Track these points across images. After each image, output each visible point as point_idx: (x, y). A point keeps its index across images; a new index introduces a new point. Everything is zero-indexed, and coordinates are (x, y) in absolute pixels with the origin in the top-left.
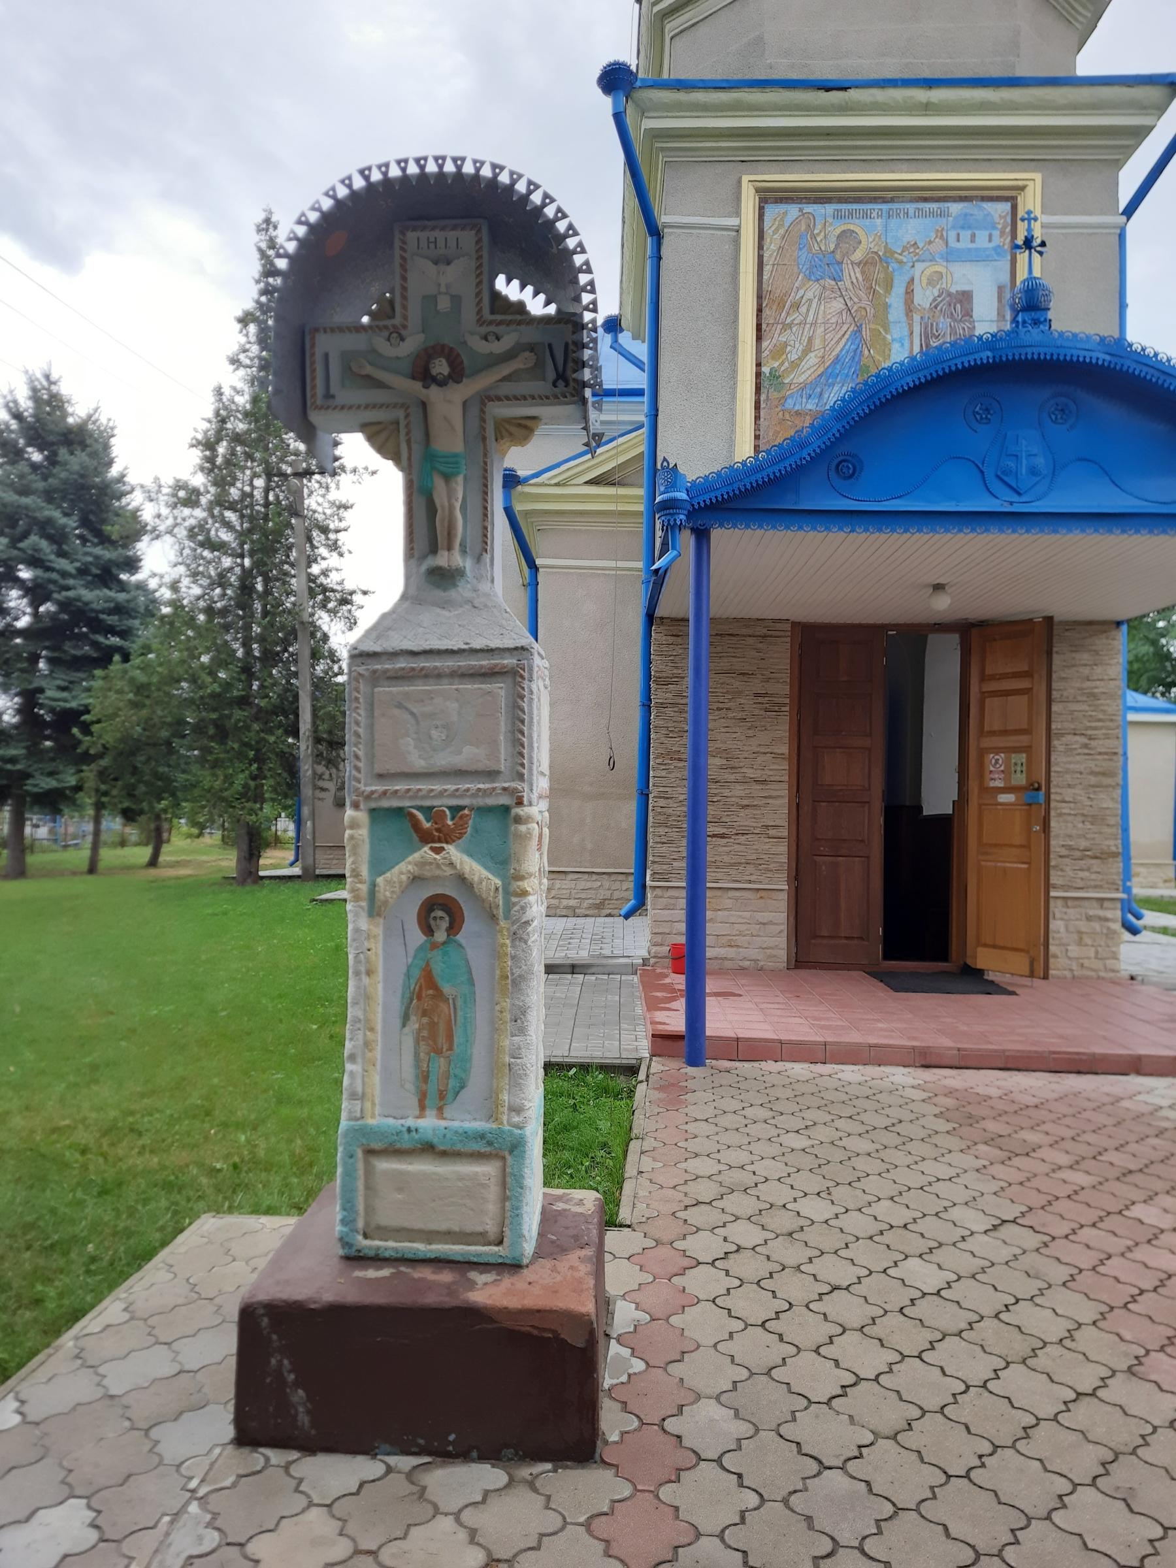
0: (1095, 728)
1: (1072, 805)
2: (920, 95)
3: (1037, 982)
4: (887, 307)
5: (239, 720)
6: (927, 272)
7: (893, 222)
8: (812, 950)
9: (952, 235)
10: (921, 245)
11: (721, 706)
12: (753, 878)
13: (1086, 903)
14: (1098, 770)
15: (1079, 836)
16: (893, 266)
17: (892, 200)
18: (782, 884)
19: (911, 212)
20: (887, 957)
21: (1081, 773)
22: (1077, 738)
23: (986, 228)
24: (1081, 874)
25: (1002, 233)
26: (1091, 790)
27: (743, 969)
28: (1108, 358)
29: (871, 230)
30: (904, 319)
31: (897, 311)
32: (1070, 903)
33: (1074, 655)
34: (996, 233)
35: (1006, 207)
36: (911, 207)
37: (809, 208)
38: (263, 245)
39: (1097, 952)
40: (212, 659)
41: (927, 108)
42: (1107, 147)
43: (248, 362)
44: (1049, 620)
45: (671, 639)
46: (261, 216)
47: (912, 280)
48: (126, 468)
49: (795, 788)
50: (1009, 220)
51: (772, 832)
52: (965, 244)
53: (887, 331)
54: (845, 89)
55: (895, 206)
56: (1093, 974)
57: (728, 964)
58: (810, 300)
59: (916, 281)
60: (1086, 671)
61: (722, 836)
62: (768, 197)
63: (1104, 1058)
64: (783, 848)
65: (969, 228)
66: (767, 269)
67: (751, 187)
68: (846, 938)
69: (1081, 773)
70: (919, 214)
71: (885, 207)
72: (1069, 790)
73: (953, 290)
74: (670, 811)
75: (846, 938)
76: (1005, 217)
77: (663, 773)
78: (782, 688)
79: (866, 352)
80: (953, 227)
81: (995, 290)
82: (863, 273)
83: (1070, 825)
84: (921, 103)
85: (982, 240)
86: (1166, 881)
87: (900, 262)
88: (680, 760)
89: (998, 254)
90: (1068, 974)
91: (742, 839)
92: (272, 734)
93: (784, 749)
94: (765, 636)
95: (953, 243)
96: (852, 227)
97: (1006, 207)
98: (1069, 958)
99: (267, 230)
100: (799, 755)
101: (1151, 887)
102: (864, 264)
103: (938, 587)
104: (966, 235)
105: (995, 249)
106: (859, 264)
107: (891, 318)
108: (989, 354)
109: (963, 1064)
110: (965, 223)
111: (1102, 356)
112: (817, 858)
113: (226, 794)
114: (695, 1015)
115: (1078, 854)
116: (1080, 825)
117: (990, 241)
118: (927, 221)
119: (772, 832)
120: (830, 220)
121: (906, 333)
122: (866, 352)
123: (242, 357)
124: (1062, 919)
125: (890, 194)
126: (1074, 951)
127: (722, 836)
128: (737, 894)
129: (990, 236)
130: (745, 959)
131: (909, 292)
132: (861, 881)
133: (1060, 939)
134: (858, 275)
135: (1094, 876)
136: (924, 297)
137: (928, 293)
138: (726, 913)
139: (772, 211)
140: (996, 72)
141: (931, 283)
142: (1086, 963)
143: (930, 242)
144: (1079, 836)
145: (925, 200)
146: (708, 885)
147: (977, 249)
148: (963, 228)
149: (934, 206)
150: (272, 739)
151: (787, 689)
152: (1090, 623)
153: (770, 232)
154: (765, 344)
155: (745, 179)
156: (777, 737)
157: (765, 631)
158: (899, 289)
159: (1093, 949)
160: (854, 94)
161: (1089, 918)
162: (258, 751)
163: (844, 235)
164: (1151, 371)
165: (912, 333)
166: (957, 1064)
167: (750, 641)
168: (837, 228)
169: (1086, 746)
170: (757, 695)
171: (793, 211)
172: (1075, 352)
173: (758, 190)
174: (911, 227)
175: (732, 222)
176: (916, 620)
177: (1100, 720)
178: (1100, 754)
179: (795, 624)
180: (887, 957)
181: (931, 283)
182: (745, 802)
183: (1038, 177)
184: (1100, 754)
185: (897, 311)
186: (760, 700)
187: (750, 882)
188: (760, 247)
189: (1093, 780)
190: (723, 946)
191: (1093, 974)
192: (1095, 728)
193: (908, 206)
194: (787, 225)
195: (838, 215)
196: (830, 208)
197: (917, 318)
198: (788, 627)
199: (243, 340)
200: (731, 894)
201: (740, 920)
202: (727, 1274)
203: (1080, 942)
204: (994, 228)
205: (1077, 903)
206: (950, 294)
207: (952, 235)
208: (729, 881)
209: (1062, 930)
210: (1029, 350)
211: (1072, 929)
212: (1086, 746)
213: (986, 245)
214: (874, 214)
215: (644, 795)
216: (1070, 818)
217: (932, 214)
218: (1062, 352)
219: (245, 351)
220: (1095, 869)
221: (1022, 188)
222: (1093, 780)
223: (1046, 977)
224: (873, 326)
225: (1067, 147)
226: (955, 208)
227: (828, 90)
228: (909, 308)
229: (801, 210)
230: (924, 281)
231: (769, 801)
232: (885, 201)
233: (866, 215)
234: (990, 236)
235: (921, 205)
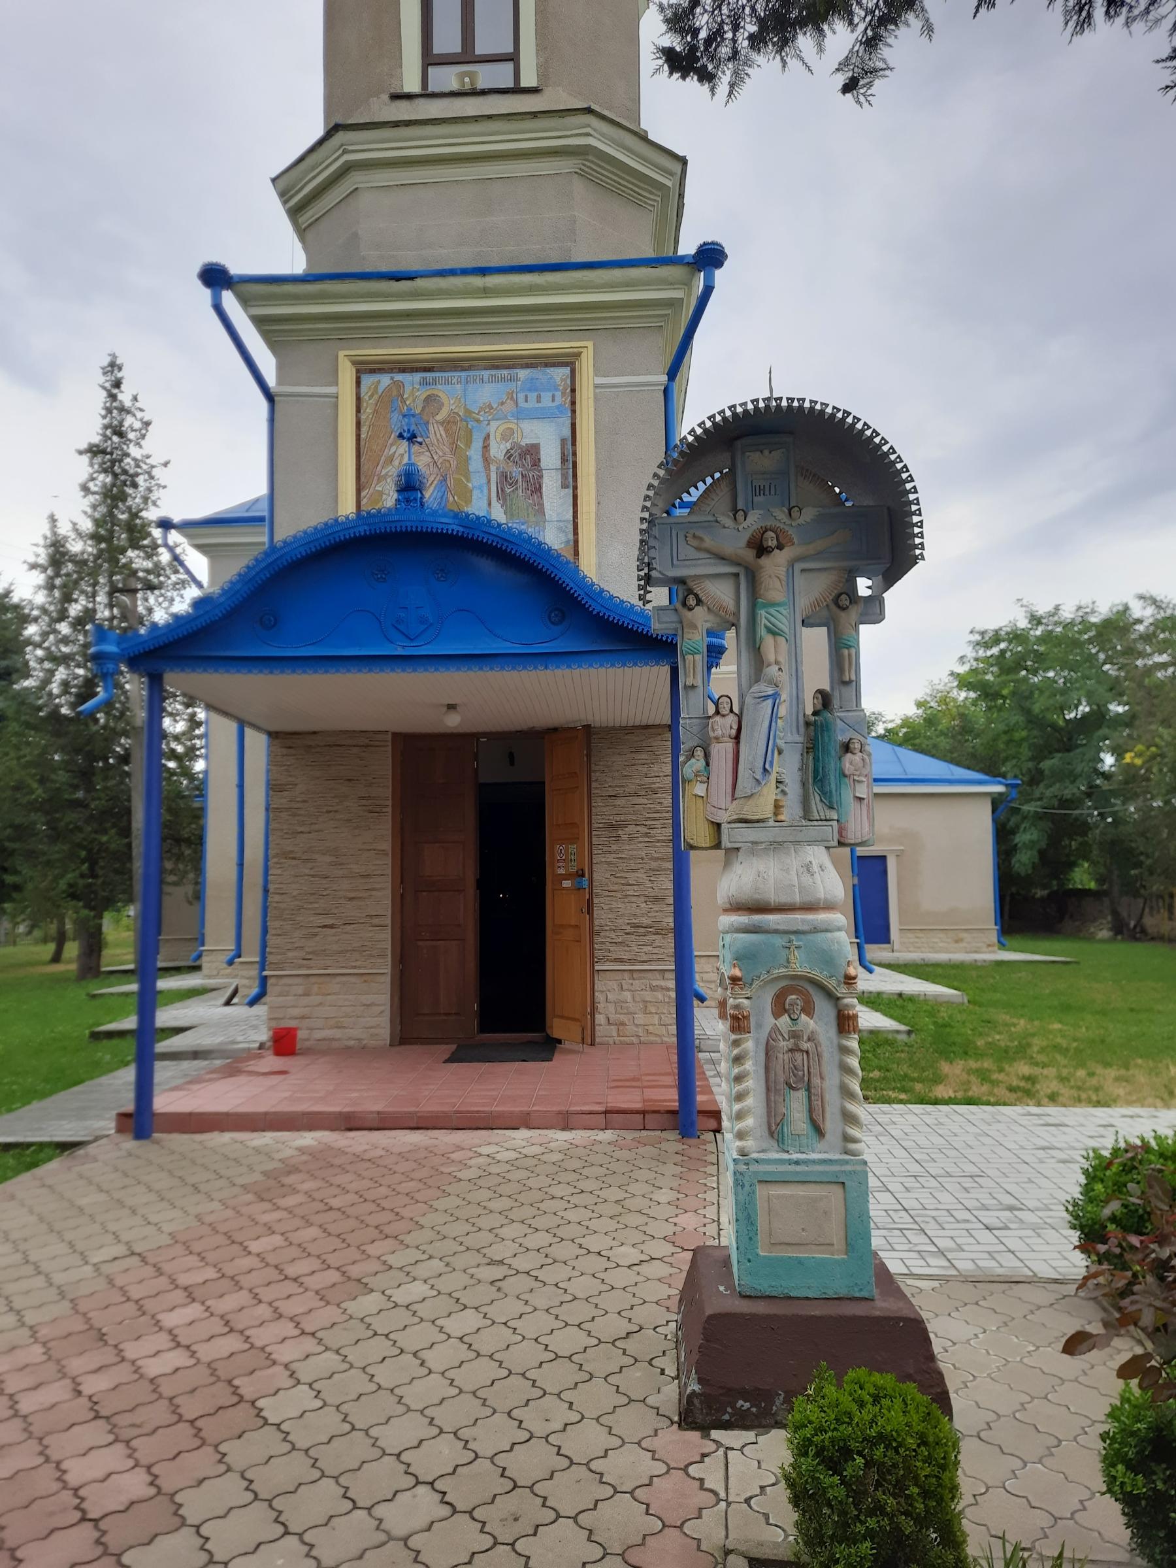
0: (654, 819)
1: (635, 888)
2: (477, 281)
3: (587, 1049)
4: (467, 459)
5: (71, 822)
6: (502, 428)
7: (471, 387)
8: (413, 1027)
9: (521, 396)
10: (495, 406)
11: (330, 808)
12: (358, 964)
13: (649, 975)
14: (656, 855)
15: (643, 915)
16: (471, 424)
17: (469, 368)
18: (385, 967)
19: (486, 378)
20: (483, 1029)
21: (642, 859)
22: (639, 828)
23: (549, 390)
24: (645, 949)
25: (563, 394)
26: (652, 873)
27: (348, 1048)
28: (461, 529)
29: (452, 393)
30: (482, 469)
31: (476, 464)
32: (635, 975)
33: (633, 755)
34: (558, 394)
35: (567, 371)
36: (486, 374)
37: (399, 377)
38: (108, 385)
39: (660, 1019)
40: (63, 761)
41: (486, 292)
42: (650, 316)
43: (96, 489)
44: (588, 727)
45: (285, 751)
46: (106, 361)
47: (488, 435)
48: (12, 584)
49: (399, 881)
50: (569, 382)
51: (376, 921)
52: (532, 404)
53: (468, 480)
54: (411, 278)
55: (471, 373)
56: (658, 1039)
57: (335, 1045)
58: (402, 455)
59: (492, 437)
60: (645, 769)
61: (331, 927)
62: (364, 368)
63: (500, 1115)
64: (387, 935)
65: (536, 390)
66: (364, 429)
67: (349, 364)
68: (446, 1014)
69: (642, 859)
70: (493, 379)
71: (463, 374)
72: (633, 875)
73: (523, 444)
74: (283, 906)
75: (446, 1014)
76: (565, 380)
77: (279, 872)
78: (385, 792)
79: (451, 499)
80: (522, 390)
81: (558, 443)
82: (446, 431)
83: (634, 905)
84: (479, 288)
85: (546, 401)
86: (989, 946)
87: (478, 421)
88: (294, 858)
89: (561, 412)
90: (635, 1040)
91: (348, 928)
92: (106, 833)
93: (387, 845)
94: (368, 746)
95: (522, 404)
96: (435, 392)
97: (567, 371)
98: (637, 1025)
99: (112, 372)
100: (402, 850)
101: (976, 952)
102: (447, 423)
103: (451, 707)
104: (533, 396)
105: (558, 407)
106: (442, 423)
107: (471, 469)
108: (366, 528)
109: (381, 1125)
110: (532, 386)
111: (456, 528)
112: (420, 943)
113: (52, 893)
114: (144, 1088)
115: (642, 930)
116: (643, 905)
117: (553, 401)
118: (500, 385)
119: (376, 921)
120: (417, 387)
121: (484, 480)
122: (451, 499)
123: (91, 485)
124: (629, 990)
125: (466, 364)
126: (640, 1018)
127: (331, 927)
128: (344, 979)
129: (553, 396)
130: (350, 1039)
131: (486, 447)
132: (457, 961)
133: (627, 1008)
134: (443, 433)
135: (655, 951)
136: (498, 450)
137: (502, 447)
138: (334, 997)
139: (368, 381)
140: (555, 259)
141: (505, 438)
142: (651, 1028)
143: (503, 403)
144: (643, 915)
145: (497, 367)
146: (696, 953)
147: (543, 408)
148: (530, 390)
149: (505, 372)
150: (105, 839)
151: (388, 792)
152: (647, 727)
153: (367, 398)
154: (363, 494)
155: (341, 354)
156: (381, 836)
157: (367, 741)
158: (477, 445)
159: (657, 1017)
160: (420, 283)
161: (653, 989)
162: (90, 851)
163: (428, 399)
164: (496, 539)
165: (489, 481)
166: (376, 1126)
167: (355, 750)
168: (422, 394)
169: (646, 835)
170: (363, 798)
171: (385, 380)
172: (435, 525)
173: (354, 363)
174: (485, 391)
175: (331, 390)
176: (506, 729)
177: (657, 812)
178: (658, 841)
179: (395, 735)
180: (483, 1029)
181: (505, 438)
182: (352, 895)
183: (590, 344)
184: (658, 841)
185: (476, 464)
186: (364, 802)
187: (355, 967)
188: (358, 410)
189: (654, 864)
190: (331, 1028)
191: (658, 1039)
192: (654, 819)
193: (483, 372)
194: (380, 391)
195: (424, 383)
196: (417, 377)
197: (493, 468)
198: (389, 737)
199: (91, 470)
200: (339, 979)
201: (347, 1003)
202: (625, 1350)
203: (645, 1011)
204: (557, 390)
205: (642, 975)
206: (520, 447)
207: (521, 396)
208: (294, 968)
209: (629, 999)
210: (394, 525)
211: (638, 999)
212: (646, 835)
213: (551, 404)
214: (455, 380)
215: (266, 891)
216: (634, 899)
217: (503, 379)
218: (425, 525)
219: (93, 479)
220: (657, 944)
221: (579, 355)
222: (654, 864)
223: (593, 1044)
224: (456, 476)
225: (611, 318)
226: (523, 374)
227: (398, 279)
228: (487, 460)
229: (392, 378)
230: (499, 436)
231: (373, 893)
232: (463, 369)
233: (448, 382)
234: (553, 396)
235: (493, 372)
